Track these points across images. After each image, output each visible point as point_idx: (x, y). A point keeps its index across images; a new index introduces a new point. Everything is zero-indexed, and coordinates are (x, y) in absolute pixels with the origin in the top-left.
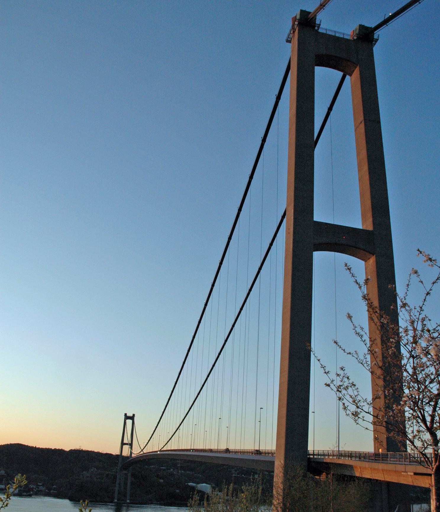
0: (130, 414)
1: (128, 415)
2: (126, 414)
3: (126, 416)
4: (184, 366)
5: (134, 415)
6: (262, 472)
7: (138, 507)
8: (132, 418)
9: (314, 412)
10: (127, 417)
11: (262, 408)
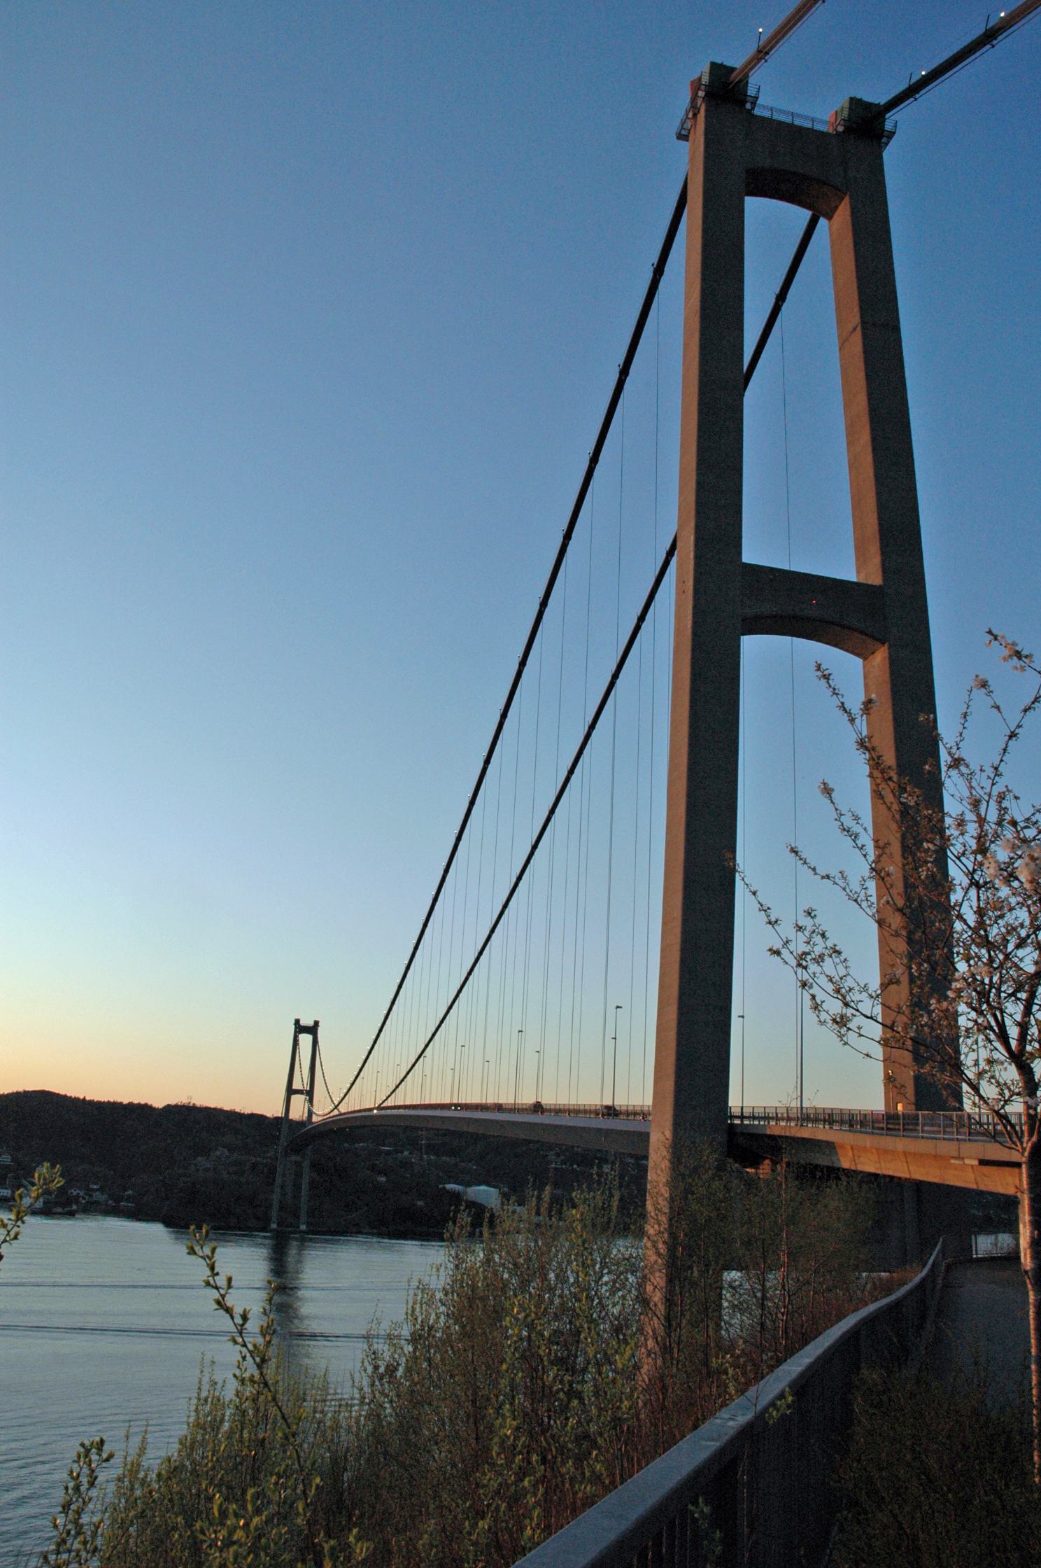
0: (307, 1021)
1: (303, 1023)
2: (297, 1022)
5: (316, 1023)
8: (313, 1030)
9: (743, 1017)
10: (300, 1029)
11: (621, 1007)
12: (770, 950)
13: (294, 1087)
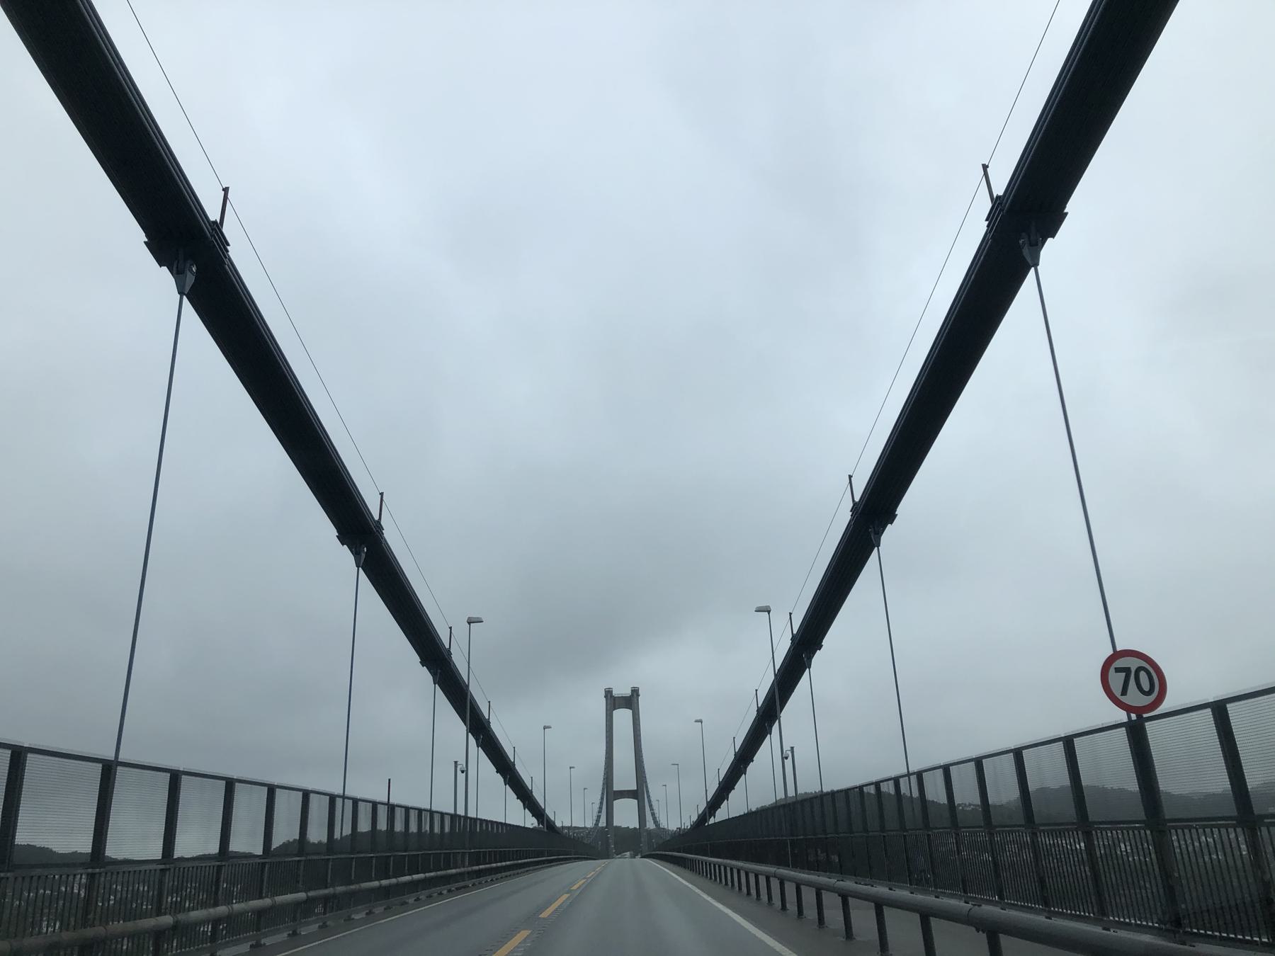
0: (622, 690)
1: (616, 693)
2: (608, 693)
3: (612, 696)
4: (136, 646)
5: (635, 692)
6: (170, 869)
7: (851, 891)
8: (631, 701)
9: (701, 721)
10: (614, 702)
11: (549, 727)
12: (756, 611)
13: (615, 789)
